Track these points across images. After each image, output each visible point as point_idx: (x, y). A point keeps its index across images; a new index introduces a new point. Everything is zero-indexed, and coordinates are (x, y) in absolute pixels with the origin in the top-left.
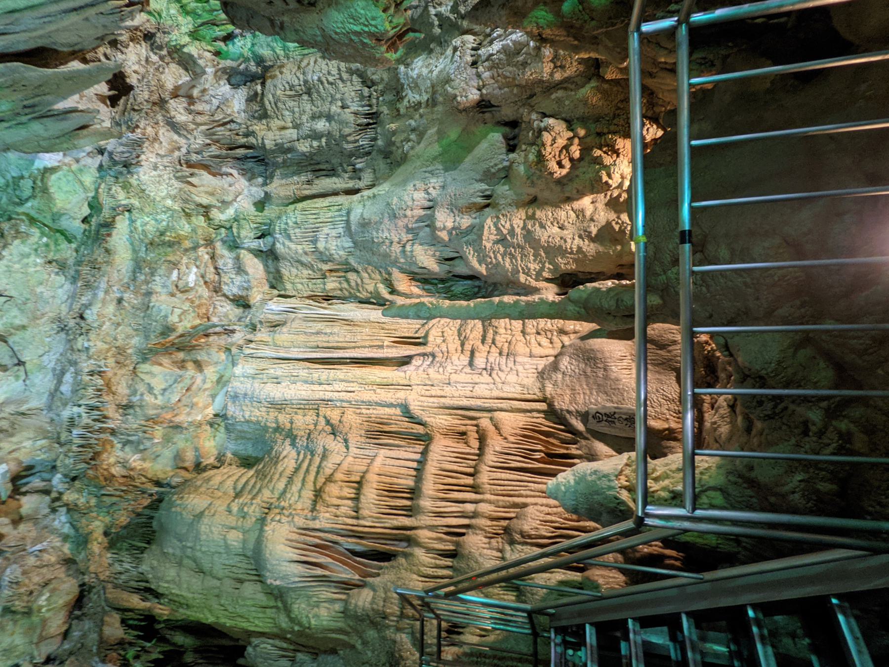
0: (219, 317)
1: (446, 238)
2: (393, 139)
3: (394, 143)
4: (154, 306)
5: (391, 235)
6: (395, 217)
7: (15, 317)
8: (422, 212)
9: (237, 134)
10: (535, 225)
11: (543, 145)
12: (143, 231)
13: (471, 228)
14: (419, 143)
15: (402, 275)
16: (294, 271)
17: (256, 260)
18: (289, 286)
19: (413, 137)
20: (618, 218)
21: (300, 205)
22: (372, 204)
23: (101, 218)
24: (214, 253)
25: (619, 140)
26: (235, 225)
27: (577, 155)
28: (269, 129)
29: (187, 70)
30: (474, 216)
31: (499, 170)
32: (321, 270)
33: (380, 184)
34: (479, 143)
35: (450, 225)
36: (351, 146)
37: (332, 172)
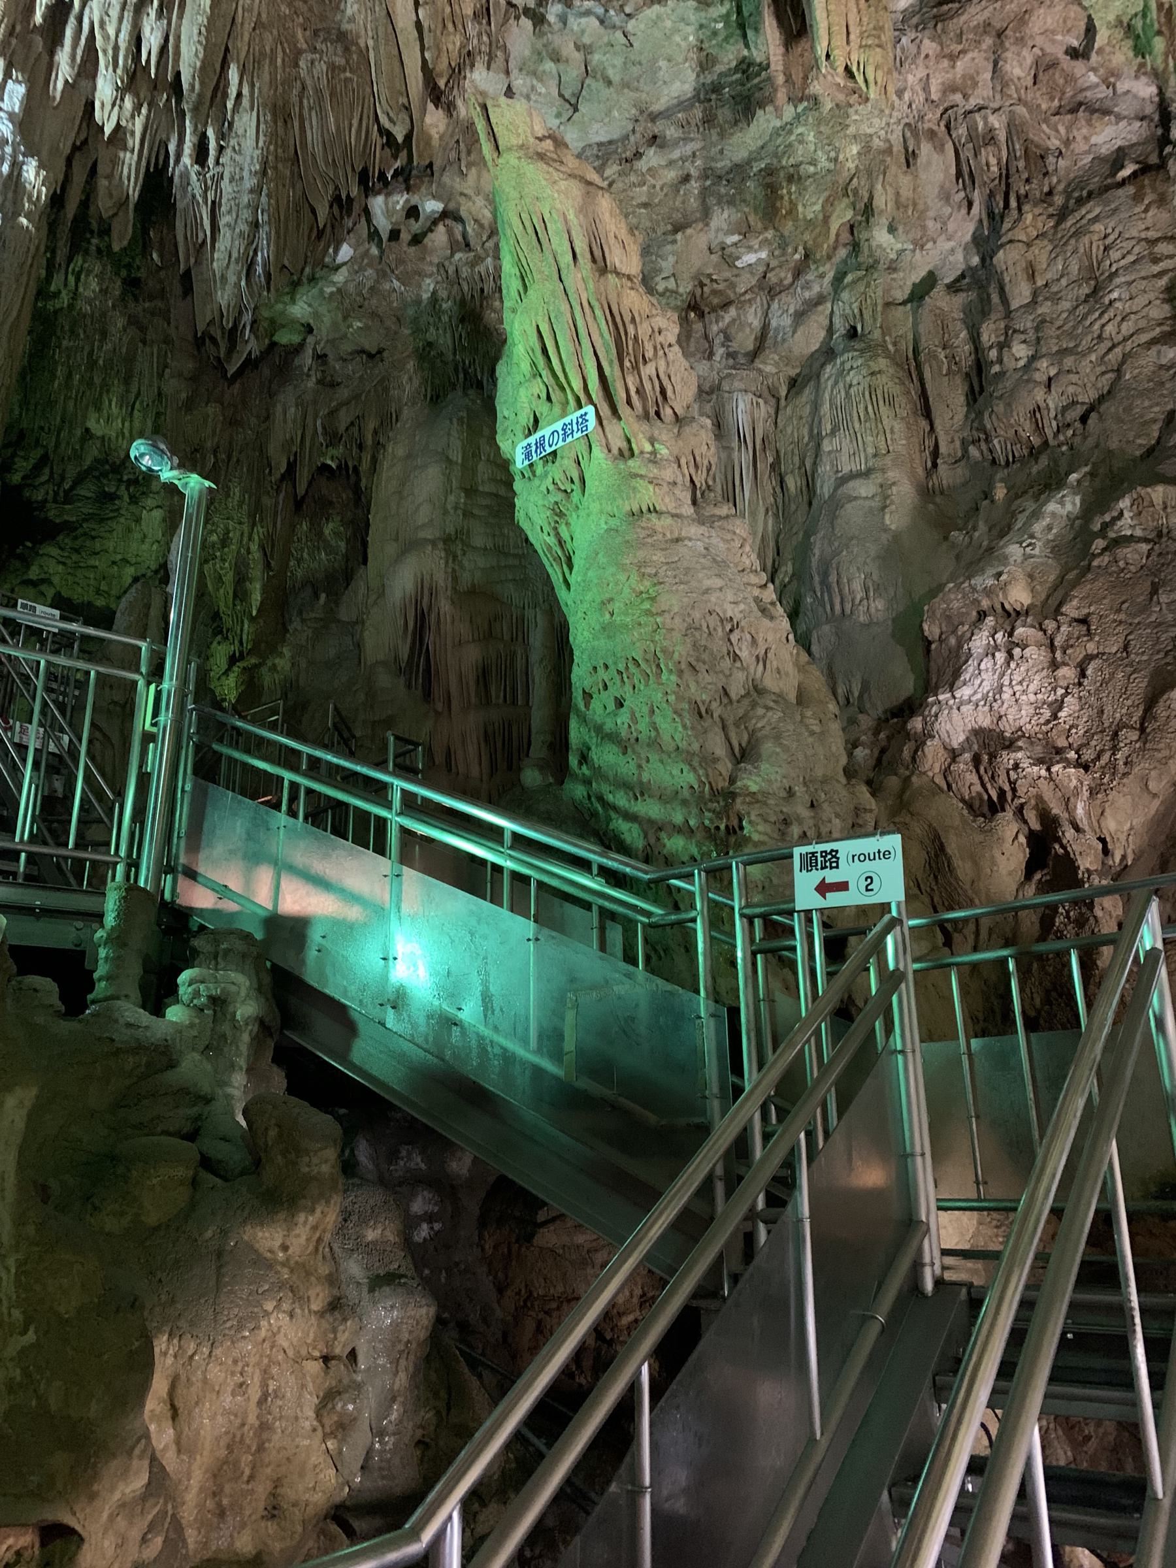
7: (614, 66)
12: (790, 145)
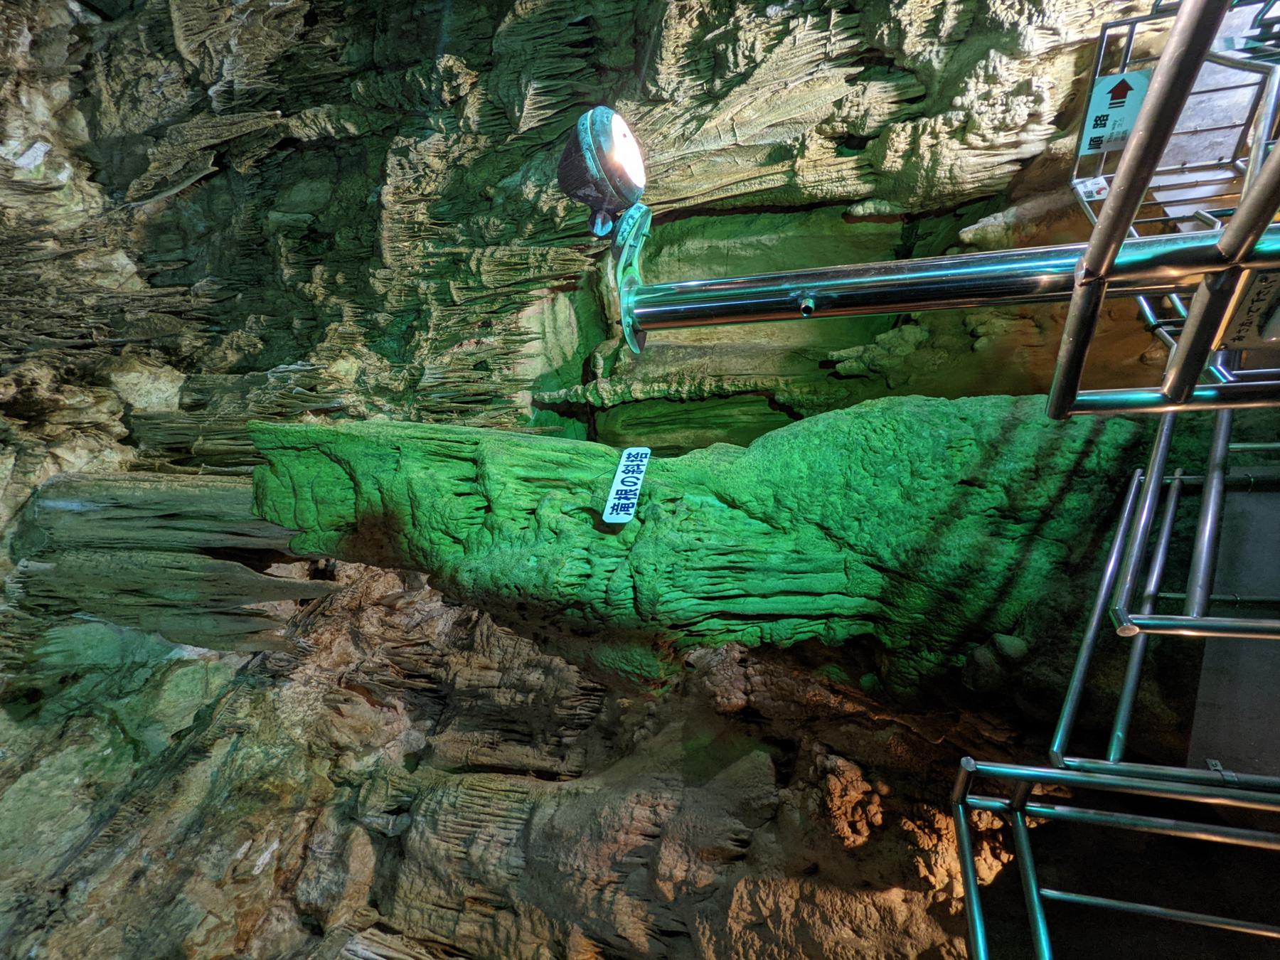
0: (265, 939)
1: (670, 896)
2: (622, 718)
3: (621, 724)
4: (181, 901)
5: (586, 865)
6: (600, 838)
8: (641, 841)
9: (426, 661)
10: (814, 915)
11: (830, 793)
12: (241, 766)
13: (713, 888)
14: (656, 734)
15: (585, 942)
16: (419, 883)
17: (370, 848)
18: (399, 910)
19: (648, 723)
20: (951, 943)
21: (470, 778)
22: (570, 806)
23: (200, 738)
24: (315, 820)
25: (938, 816)
26: (367, 784)
27: (878, 819)
28: (468, 664)
29: (404, 582)
30: (719, 869)
31: (763, 806)
32: (461, 894)
33: (588, 776)
34: (738, 759)
35: (679, 874)
36: (564, 712)
37: (527, 739)
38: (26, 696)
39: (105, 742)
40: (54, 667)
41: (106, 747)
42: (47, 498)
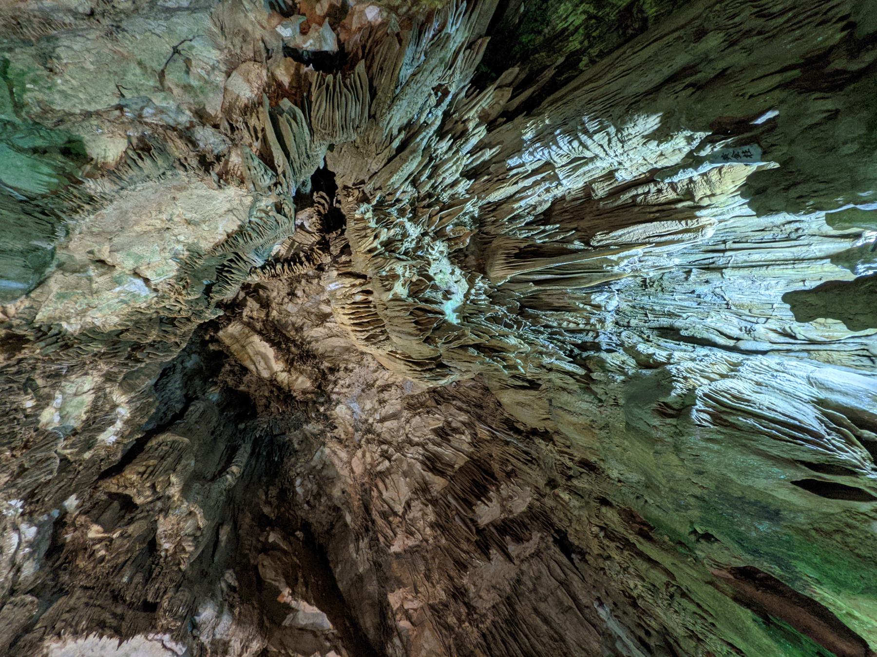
38: (70, 153)
39: (29, 94)
40: (48, 164)
41: (30, 90)
42: (21, 289)
